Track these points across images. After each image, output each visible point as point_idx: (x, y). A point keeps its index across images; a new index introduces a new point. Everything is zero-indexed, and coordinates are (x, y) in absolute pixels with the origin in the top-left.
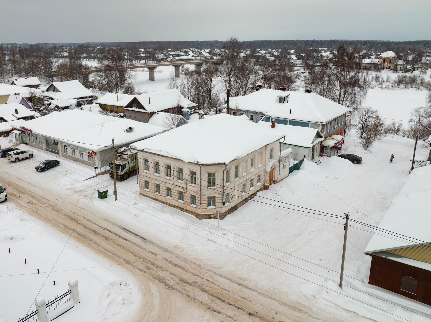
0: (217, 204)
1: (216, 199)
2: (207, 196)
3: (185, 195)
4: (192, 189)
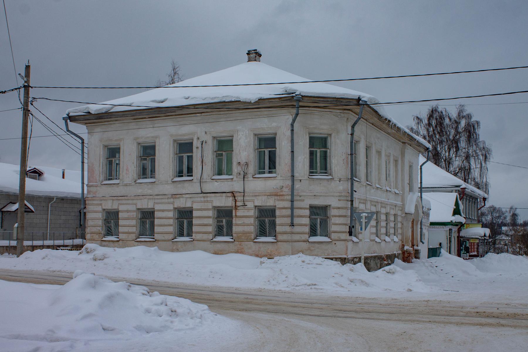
0: (334, 228)
1: (333, 212)
2: (307, 203)
3: (240, 213)
4: (261, 189)
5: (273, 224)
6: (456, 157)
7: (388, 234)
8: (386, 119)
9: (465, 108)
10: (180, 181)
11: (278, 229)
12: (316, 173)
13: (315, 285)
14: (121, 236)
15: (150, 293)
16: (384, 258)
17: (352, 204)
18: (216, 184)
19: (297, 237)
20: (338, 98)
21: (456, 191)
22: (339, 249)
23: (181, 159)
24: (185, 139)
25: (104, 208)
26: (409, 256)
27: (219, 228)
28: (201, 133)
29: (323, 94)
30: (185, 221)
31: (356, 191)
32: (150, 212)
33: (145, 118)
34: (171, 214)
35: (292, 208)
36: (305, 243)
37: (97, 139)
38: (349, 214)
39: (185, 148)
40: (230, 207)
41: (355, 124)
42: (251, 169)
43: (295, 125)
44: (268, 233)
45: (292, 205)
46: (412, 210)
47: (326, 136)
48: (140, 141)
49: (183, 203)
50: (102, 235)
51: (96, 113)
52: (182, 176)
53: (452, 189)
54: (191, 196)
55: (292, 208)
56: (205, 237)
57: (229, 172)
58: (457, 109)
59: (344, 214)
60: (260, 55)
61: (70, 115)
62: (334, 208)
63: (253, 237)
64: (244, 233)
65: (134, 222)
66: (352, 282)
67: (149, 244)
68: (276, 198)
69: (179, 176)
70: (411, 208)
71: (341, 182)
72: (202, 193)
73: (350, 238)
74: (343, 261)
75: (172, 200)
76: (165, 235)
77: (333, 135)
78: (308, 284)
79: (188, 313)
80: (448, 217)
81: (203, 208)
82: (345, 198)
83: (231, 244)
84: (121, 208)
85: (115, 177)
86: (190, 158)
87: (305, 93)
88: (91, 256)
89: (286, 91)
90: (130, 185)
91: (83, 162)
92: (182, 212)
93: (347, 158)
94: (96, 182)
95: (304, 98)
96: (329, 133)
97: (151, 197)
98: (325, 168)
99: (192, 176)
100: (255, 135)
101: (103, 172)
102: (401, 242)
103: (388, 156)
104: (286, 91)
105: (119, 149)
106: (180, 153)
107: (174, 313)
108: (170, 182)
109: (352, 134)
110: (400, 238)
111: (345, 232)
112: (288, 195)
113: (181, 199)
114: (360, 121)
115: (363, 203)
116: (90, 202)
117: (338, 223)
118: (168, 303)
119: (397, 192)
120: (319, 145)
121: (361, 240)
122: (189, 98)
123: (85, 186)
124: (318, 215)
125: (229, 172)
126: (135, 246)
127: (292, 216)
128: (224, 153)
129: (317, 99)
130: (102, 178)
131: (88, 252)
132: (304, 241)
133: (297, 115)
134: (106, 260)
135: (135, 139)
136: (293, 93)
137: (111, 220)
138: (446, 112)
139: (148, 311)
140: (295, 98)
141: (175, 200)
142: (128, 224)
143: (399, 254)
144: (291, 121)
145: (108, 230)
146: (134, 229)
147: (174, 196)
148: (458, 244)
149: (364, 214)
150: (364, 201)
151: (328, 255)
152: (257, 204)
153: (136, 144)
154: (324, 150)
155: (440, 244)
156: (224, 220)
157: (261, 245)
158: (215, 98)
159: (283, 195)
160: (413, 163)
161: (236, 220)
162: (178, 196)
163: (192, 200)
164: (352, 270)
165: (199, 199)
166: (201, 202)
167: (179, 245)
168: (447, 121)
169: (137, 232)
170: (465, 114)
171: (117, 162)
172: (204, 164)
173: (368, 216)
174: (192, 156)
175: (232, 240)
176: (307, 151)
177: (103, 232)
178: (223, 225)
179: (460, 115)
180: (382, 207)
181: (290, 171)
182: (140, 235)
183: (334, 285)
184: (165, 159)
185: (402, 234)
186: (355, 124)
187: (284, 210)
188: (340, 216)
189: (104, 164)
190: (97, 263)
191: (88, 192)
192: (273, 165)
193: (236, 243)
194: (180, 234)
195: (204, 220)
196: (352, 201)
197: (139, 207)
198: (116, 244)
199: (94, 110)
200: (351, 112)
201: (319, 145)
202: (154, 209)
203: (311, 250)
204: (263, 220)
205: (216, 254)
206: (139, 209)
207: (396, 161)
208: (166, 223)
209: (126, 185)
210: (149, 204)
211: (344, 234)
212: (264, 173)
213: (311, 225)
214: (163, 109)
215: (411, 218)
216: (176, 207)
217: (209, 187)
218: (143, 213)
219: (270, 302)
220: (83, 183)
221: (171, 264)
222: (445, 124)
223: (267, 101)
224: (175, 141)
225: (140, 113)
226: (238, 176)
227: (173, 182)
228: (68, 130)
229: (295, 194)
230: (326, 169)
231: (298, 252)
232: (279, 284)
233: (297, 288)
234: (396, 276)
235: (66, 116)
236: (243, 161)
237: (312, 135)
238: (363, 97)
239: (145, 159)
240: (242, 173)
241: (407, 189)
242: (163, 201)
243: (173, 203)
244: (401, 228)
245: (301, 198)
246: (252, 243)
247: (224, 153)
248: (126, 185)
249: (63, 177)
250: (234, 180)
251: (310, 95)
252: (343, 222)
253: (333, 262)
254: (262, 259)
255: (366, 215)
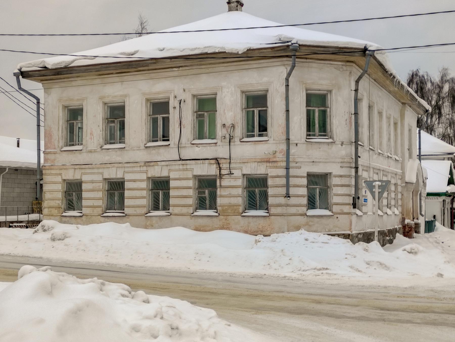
0: (335, 199)
1: (334, 181)
2: (304, 171)
3: (225, 182)
4: (250, 156)
5: (265, 196)
6: (439, 123)
7: (389, 206)
8: (391, 74)
9: (449, 72)
10: (154, 147)
11: (271, 200)
12: (314, 135)
13: (327, 269)
14: (85, 211)
15: (133, 293)
16: (386, 234)
17: (357, 172)
18: (197, 149)
19: (293, 210)
20: (340, 48)
21: (448, 159)
22: (342, 224)
23: (155, 121)
24: (160, 97)
25: (64, 178)
26: (411, 231)
27: (200, 200)
28: (179, 89)
29: (323, 42)
30: (161, 193)
31: (360, 157)
32: (119, 183)
33: (112, 74)
34: (144, 185)
35: (288, 177)
36: (303, 217)
37: (55, 99)
38: (353, 183)
39: (159, 108)
40: (214, 176)
41: (360, 78)
42: (239, 132)
43: (291, 79)
44: (258, 206)
45: (288, 173)
46: (414, 180)
47: (325, 92)
48: (107, 100)
49: (158, 172)
50: (62, 210)
51: (54, 67)
52: (157, 141)
53: (445, 156)
54: (167, 163)
55: (288, 177)
56: (185, 210)
57: (212, 136)
58: (440, 72)
59: (347, 183)
60: (242, 5)
61: (22, 70)
62: (336, 176)
63: (241, 211)
64: (231, 206)
65: (100, 195)
66: (368, 264)
67: (118, 219)
68: (268, 164)
69: (153, 141)
70: (411, 177)
71: (344, 146)
72: (181, 160)
73: (353, 211)
74: (353, 238)
75: (145, 168)
76: (137, 209)
77: (334, 92)
78: (318, 268)
79: (197, 330)
80: (444, 187)
81: (181, 177)
82: (348, 165)
83: (215, 219)
84: (84, 178)
85: (77, 143)
86: (166, 121)
87: (303, 41)
88: (48, 235)
89: (280, 40)
90: (95, 151)
91: (39, 126)
92: (157, 182)
93: (351, 118)
94: (55, 149)
95: (301, 47)
96: (330, 89)
97: (120, 165)
98: (324, 129)
99: (168, 140)
100: (243, 92)
101: (62, 136)
102: (401, 215)
103: (389, 118)
104: (280, 40)
105: (82, 110)
106: (154, 114)
107: (175, 332)
108: (143, 147)
109: (356, 91)
110: (401, 211)
111: (348, 204)
112: (282, 161)
113: (156, 167)
114: (364, 78)
115: (366, 171)
116: (48, 172)
117: (339, 194)
118: (165, 316)
119: (397, 158)
120: (318, 103)
121: (365, 213)
122: (164, 49)
123: (41, 152)
124: (317, 184)
125: (212, 136)
126: (101, 222)
127: (288, 186)
128: (206, 114)
129: (316, 49)
130: (61, 143)
131: (45, 231)
132: (301, 215)
133: (293, 67)
134: (67, 241)
135: (101, 98)
136: (288, 42)
137: (73, 194)
138: (427, 75)
139: (136, 329)
140: (291, 47)
141: (149, 168)
142: (94, 196)
143: (400, 228)
144: (285, 76)
145: (69, 204)
146: (100, 203)
147: (147, 163)
148: (451, 216)
149: (377, 183)
150: (367, 168)
151: (329, 231)
152: (245, 172)
153: (101, 105)
154: (323, 109)
155: (434, 217)
156: (207, 191)
157: (251, 219)
158: (195, 49)
159: (276, 162)
160: (412, 127)
161: (220, 191)
162: (152, 164)
163: (169, 168)
164: (366, 250)
165: (177, 167)
166: (179, 170)
167: (154, 220)
168: (429, 85)
169: (104, 206)
170: (448, 78)
171: (79, 126)
172: (182, 127)
173: (382, 185)
174: (168, 118)
175: (217, 214)
176: (304, 109)
177: (63, 207)
178: (205, 197)
179: (443, 80)
180: (383, 175)
181: (285, 134)
182: (107, 209)
183: (350, 269)
184: (137, 121)
185: (402, 206)
186: (360, 78)
187: (277, 179)
188: (342, 186)
189: (64, 127)
190: (56, 243)
191: (45, 160)
192: (263, 129)
193: (221, 217)
194: (154, 207)
195: (183, 192)
196: (357, 168)
197: (106, 176)
198: (79, 220)
199: (51, 63)
200: (354, 65)
201: (318, 103)
202: (124, 179)
203: (310, 226)
204: (252, 191)
205: (197, 230)
206: (106, 179)
207: (395, 124)
208: (137, 194)
209: (90, 152)
210: (118, 173)
211: (348, 207)
212: (253, 136)
213: (309, 197)
214: (134, 63)
215: (412, 188)
216: (150, 176)
217: (188, 153)
218: (111, 184)
219: (281, 294)
220: (39, 150)
221: (148, 244)
222: (427, 88)
223: (257, 51)
224: (147, 100)
225: (106, 67)
226: (223, 140)
227: (146, 147)
228: (20, 88)
229: (291, 160)
230: (325, 131)
231: (298, 228)
232: (282, 267)
233: (304, 273)
234: (419, 257)
235: (18, 71)
236: (228, 123)
237: (309, 92)
238: (371, 46)
239: (113, 122)
240: (228, 136)
241: (407, 155)
242: (135, 169)
243: (146, 172)
244: (401, 199)
245: (297, 165)
246: (240, 216)
247: (206, 114)
248: (90, 152)
249: (18, 146)
250: (217, 144)
251: (308, 44)
252: (346, 193)
253: (336, 238)
254: (257, 238)
255: (380, 183)
